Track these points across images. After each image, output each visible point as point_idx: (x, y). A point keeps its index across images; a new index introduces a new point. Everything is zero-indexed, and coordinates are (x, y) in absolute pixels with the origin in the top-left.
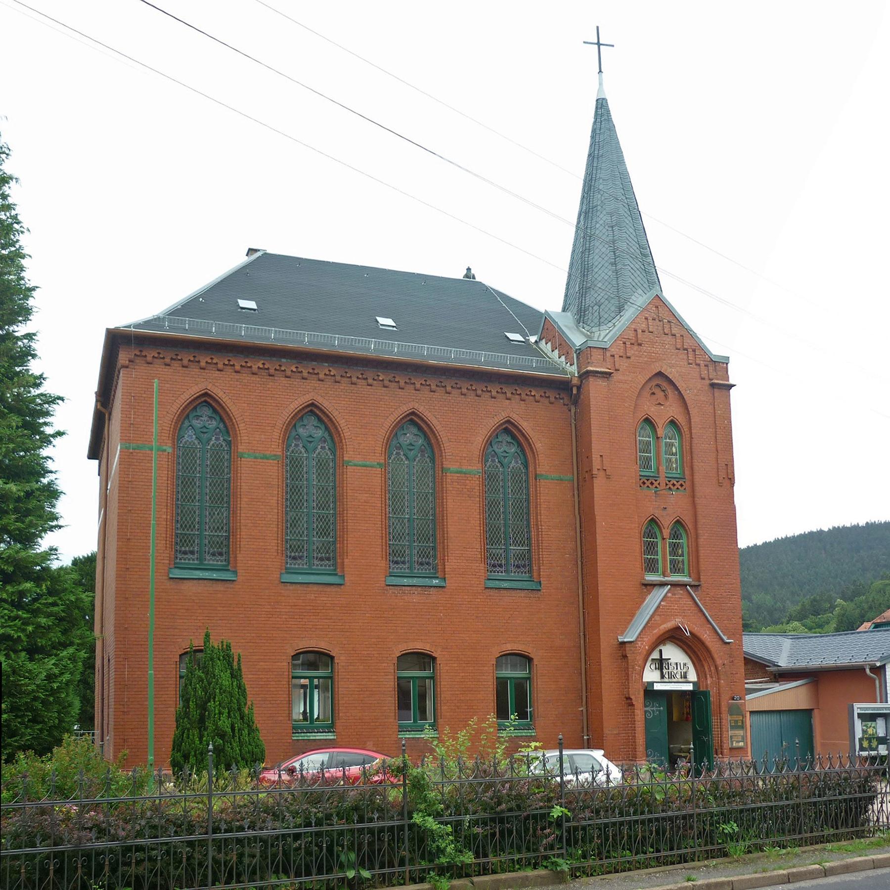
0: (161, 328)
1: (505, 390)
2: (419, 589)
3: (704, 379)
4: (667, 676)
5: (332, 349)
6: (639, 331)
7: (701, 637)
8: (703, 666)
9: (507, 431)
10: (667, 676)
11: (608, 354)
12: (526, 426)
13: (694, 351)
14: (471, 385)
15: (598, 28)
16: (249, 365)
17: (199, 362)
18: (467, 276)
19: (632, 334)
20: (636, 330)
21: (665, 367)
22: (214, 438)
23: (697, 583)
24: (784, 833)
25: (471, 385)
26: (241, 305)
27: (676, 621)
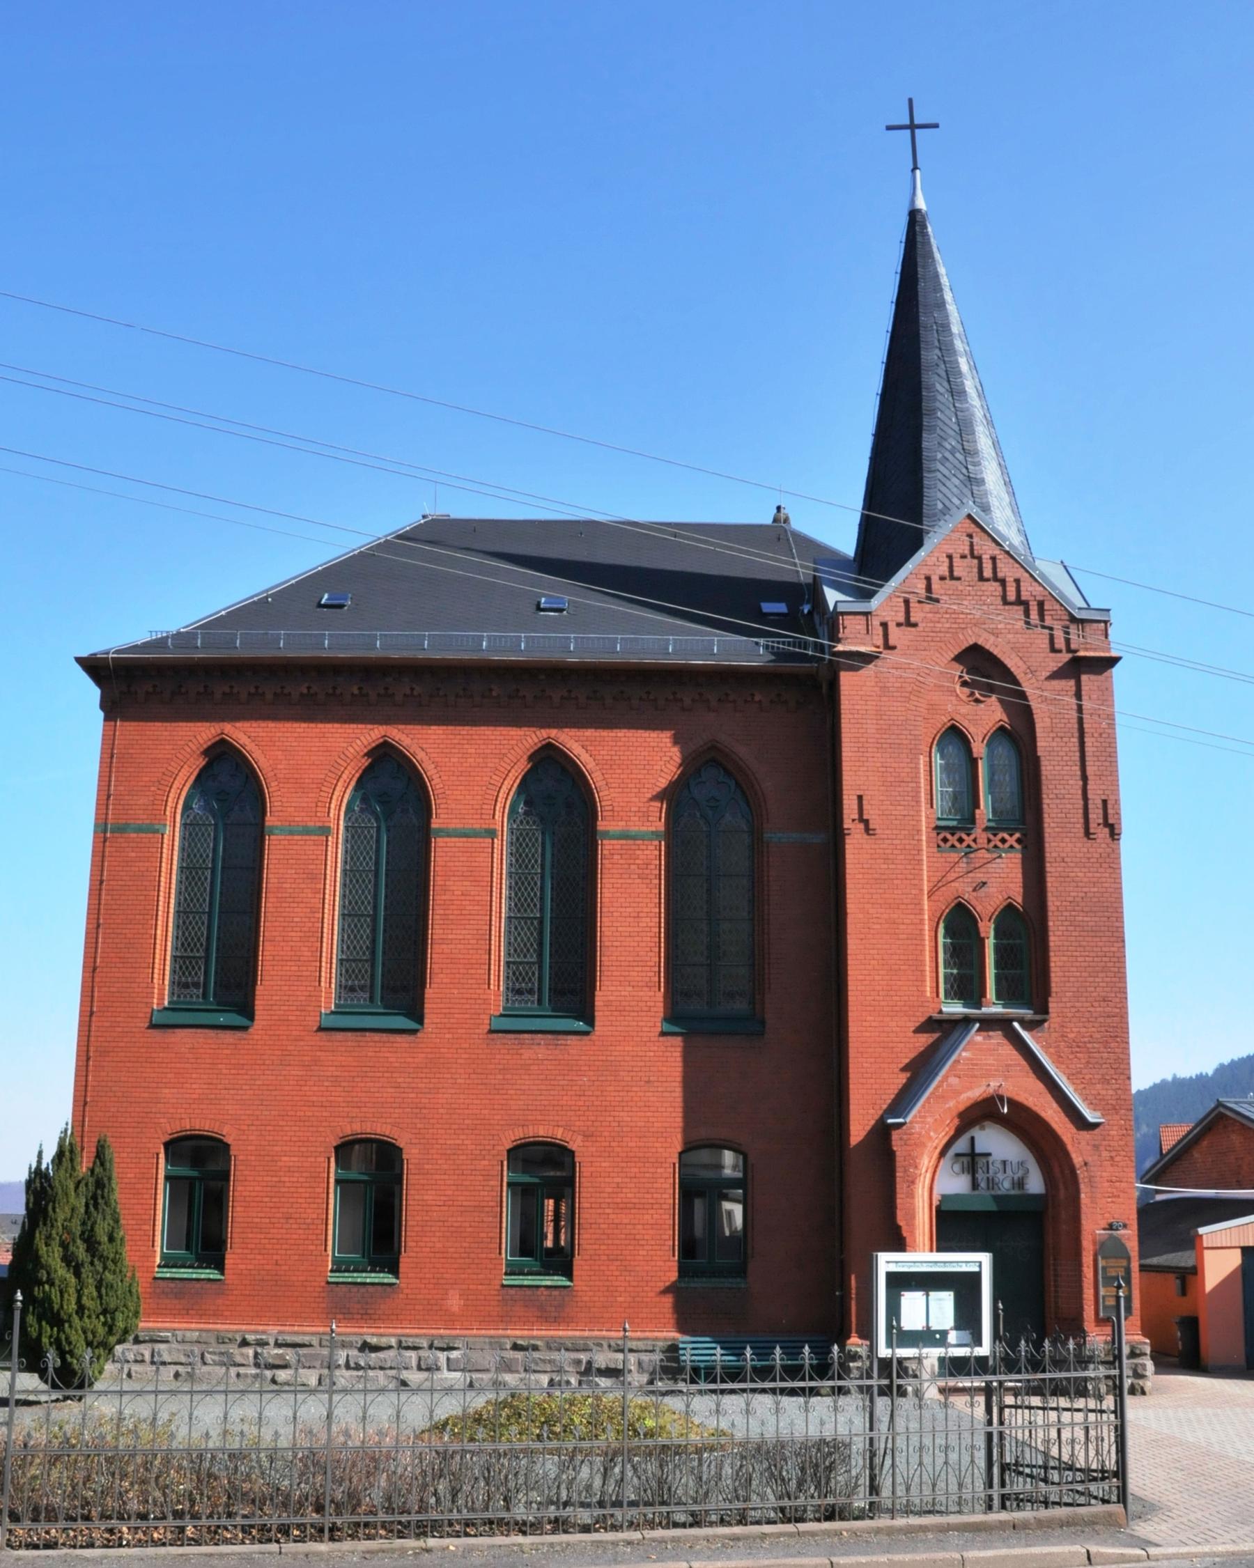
0: (166, 647)
1: (315, 689)
2: (550, 1036)
3: (1060, 651)
4: (983, 1185)
5: (372, 654)
6: (935, 579)
7: (1043, 1114)
8: (71, 1144)
9: (714, 762)
10: (983, 1185)
11: (876, 622)
12: (743, 751)
13: (1041, 604)
14: (648, 693)
15: (936, 126)
16: (286, 691)
17: (655, 700)
18: (775, 520)
19: (921, 587)
20: (928, 579)
21: (985, 635)
22: (236, 808)
23: (1038, 1017)
24: (990, 1508)
25: (648, 693)
26: (765, 610)
27: (991, 1085)
